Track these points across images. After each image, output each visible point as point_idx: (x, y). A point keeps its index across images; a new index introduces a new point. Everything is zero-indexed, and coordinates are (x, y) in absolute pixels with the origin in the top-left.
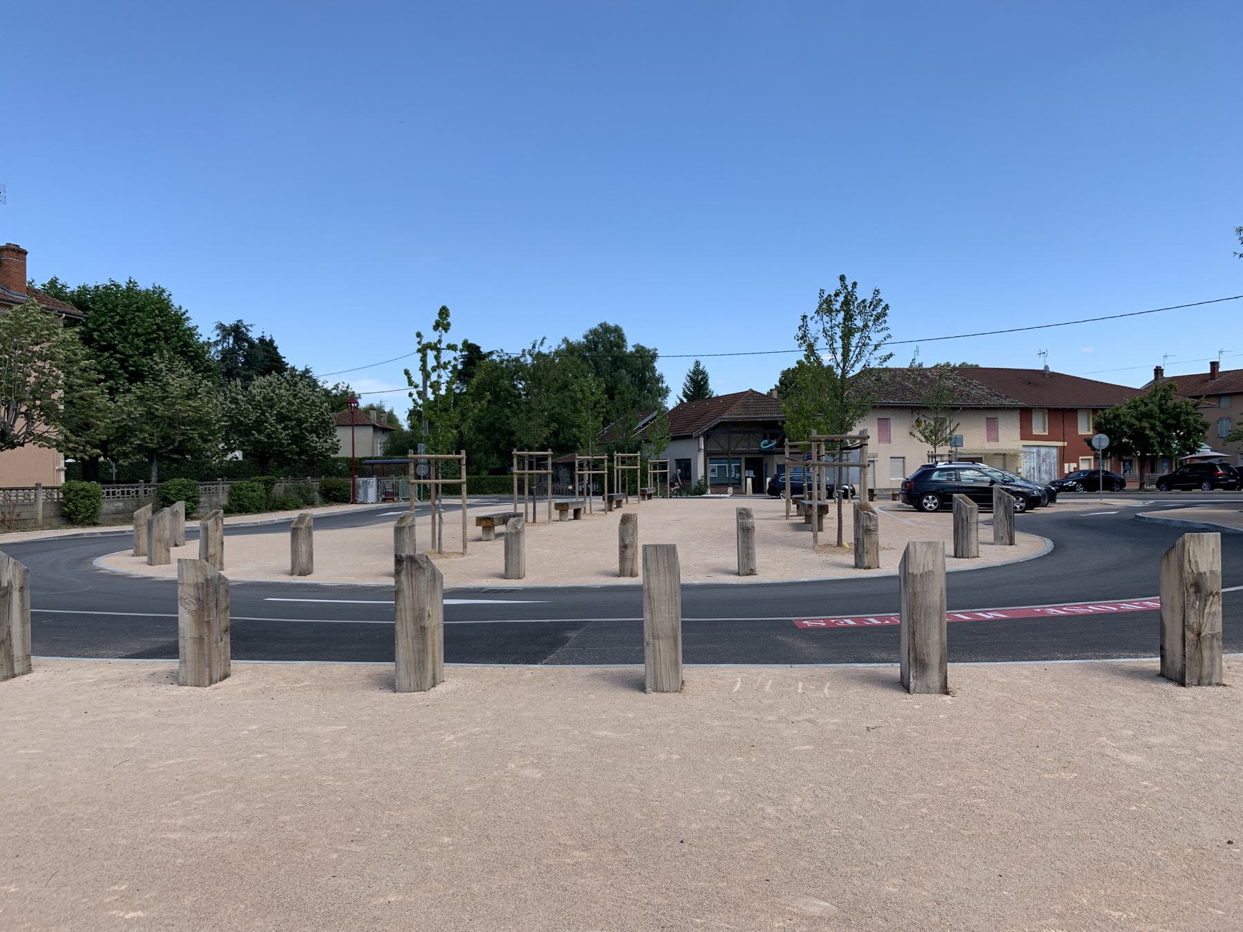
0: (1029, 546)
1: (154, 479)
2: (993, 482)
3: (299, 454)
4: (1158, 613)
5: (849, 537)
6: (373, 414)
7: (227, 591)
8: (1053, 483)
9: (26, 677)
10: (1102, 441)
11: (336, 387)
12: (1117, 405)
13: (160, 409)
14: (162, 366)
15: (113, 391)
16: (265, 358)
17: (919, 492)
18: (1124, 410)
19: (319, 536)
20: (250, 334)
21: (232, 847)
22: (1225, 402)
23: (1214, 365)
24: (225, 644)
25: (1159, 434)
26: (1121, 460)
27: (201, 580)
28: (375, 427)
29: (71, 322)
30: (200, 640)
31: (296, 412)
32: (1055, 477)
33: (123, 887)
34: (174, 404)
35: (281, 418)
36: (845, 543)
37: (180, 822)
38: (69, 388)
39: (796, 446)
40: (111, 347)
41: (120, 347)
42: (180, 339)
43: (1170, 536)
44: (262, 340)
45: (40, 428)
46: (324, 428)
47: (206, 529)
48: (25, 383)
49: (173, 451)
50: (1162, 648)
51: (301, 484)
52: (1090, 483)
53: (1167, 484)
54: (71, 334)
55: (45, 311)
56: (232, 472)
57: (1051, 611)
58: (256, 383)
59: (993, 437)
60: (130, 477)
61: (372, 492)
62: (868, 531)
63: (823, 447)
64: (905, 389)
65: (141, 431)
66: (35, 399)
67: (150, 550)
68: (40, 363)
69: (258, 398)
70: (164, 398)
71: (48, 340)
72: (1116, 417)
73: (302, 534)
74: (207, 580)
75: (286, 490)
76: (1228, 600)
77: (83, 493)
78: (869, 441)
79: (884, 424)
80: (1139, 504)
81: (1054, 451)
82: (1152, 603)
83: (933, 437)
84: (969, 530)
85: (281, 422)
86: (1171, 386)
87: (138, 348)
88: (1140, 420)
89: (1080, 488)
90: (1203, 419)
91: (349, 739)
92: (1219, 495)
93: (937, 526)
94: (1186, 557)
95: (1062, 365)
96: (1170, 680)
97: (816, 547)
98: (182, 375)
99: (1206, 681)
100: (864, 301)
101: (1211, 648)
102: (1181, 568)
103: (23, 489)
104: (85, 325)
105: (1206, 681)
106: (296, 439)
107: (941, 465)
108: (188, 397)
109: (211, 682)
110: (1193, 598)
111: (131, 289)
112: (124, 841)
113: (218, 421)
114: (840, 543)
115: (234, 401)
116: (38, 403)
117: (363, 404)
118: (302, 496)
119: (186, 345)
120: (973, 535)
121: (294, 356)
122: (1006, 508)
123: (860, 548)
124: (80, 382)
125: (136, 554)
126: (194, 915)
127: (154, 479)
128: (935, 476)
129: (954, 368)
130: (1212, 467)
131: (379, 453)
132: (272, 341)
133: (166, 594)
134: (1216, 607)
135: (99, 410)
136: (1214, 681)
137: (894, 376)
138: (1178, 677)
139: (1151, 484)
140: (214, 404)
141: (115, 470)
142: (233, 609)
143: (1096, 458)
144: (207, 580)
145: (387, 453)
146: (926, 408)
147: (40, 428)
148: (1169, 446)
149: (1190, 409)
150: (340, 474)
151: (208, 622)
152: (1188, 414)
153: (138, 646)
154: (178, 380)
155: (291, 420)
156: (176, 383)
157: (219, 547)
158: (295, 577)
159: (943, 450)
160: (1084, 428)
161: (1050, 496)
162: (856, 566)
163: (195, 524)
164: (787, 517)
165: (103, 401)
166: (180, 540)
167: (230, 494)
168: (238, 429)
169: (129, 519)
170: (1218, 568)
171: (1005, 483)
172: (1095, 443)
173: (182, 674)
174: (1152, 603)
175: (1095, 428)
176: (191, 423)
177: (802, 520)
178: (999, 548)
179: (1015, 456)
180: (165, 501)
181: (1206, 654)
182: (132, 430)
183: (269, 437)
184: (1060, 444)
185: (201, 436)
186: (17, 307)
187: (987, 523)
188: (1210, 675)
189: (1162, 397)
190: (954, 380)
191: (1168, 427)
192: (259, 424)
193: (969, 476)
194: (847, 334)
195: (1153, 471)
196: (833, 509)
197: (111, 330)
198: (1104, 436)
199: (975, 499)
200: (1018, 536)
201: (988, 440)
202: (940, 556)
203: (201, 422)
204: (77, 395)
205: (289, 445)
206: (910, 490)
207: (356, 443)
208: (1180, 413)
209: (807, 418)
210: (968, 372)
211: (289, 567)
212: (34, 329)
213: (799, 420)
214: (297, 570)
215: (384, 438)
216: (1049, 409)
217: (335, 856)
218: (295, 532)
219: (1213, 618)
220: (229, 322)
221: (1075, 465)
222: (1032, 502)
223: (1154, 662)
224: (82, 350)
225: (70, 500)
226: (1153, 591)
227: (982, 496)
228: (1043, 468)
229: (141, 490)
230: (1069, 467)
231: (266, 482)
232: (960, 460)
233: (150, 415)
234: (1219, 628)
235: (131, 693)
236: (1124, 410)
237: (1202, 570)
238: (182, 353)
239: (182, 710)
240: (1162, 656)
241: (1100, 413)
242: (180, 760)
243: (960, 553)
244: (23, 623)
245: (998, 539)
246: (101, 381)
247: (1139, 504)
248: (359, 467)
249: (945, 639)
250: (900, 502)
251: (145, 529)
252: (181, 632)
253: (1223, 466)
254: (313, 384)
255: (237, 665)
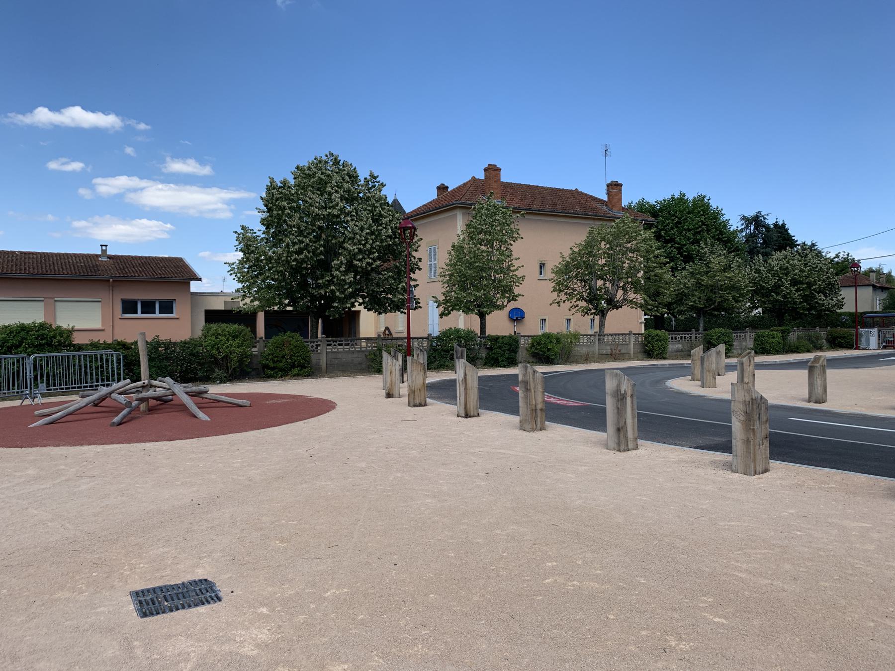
1: (701, 328)
3: (809, 310)
6: (873, 276)
7: (767, 409)
9: (635, 452)
11: (837, 256)
13: (705, 280)
14: (706, 250)
15: (674, 269)
16: (779, 238)
19: (832, 374)
20: (767, 221)
21: (785, 594)
23: (614, 188)
24: (765, 448)
27: (748, 399)
28: (874, 287)
29: (648, 226)
30: (747, 442)
31: (807, 277)
33: (710, 600)
34: (715, 276)
35: (794, 282)
37: (744, 566)
38: (648, 270)
40: (672, 240)
41: (677, 239)
42: (717, 230)
44: (776, 225)
45: (631, 296)
46: (831, 289)
47: (742, 364)
48: (622, 268)
49: (714, 309)
51: (812, 333)
54: (648, 234)
55: (634, 221)
56: (754, 324)
58: (775, 257)
60: (686, 327)
61: (874, 341)
65: (693, 296)
66: (628, 277)
67: (702, 377)
68: (631, 255)
69: (776, 268)
70: (707, 272)
71: (636, 239)
73: (817, 372)
74: (752, 399)
75: (799, 338)
77: (657, 338)
85: (794, 286)
87: (689, 239)
91: (876, 536)
98: (720, 255)
103: (612, 335)
104: (656, 227)
106: (806, 298)
108: (724, 271)
109: (755, 474)
111: (682, 199)
112: (707, 569)
113: (746, 287)
115: (758, 271)
116: (630, 280)
117: (864, 267)
118: (812, 342)
119: (721, 233)
121: (801, 234)
124: (655, 265)
125: (693, 379)
126: (762, 634)
127: (701, 328)
131: (878, 308)
132: (784, 225)
133: (722, 408)
135: (666, 283)
140: (743, 275)
141: (674, 323)
142: (772, 422)
144: (752, 399)
145: (886, 308)
147: (631, 296)
150: (843, 325)
151: (753, 430)
153: (701, 442)
154: (717, 258)
155: (803, 284)
156: (716, 261)
157: (751, 378)
158: (811, 404)
163: (733, 361)
165: (668, 276)
166: (722, 371)
167: (755, 340)
168: (760, 292)
169: (689, 356)
173: (735, 463)
176: (727, 289)
180: (709, 345)
182: (686, 295)
183: (785, 297)
185: (734, 298)
186: (618, 221)
192: (777, 288)
197: (672, 229)
203: (734, 288)
204: (653, 274)
205: (801, 303)
207: (856, 300)
211: (807, 396)
212: (628, 233)
214: (813, 399)
215: (884, 295)
217: (872, 624)
218: (811, 369)
220: (750, 214)
224: (655, 244)
225: (649, 342)
229: (693, 336)
231: (783, 332)
233: (699, 285)
235: (700, 471)
238: (718, 239)
239: (736, 489)
242: (739, 524)
244: (633, 418)
246: (667, 263)
248: (861, 320)
251: (698, 363)
252: (733, 435)
254: (819, 254)
255: (774, 464)
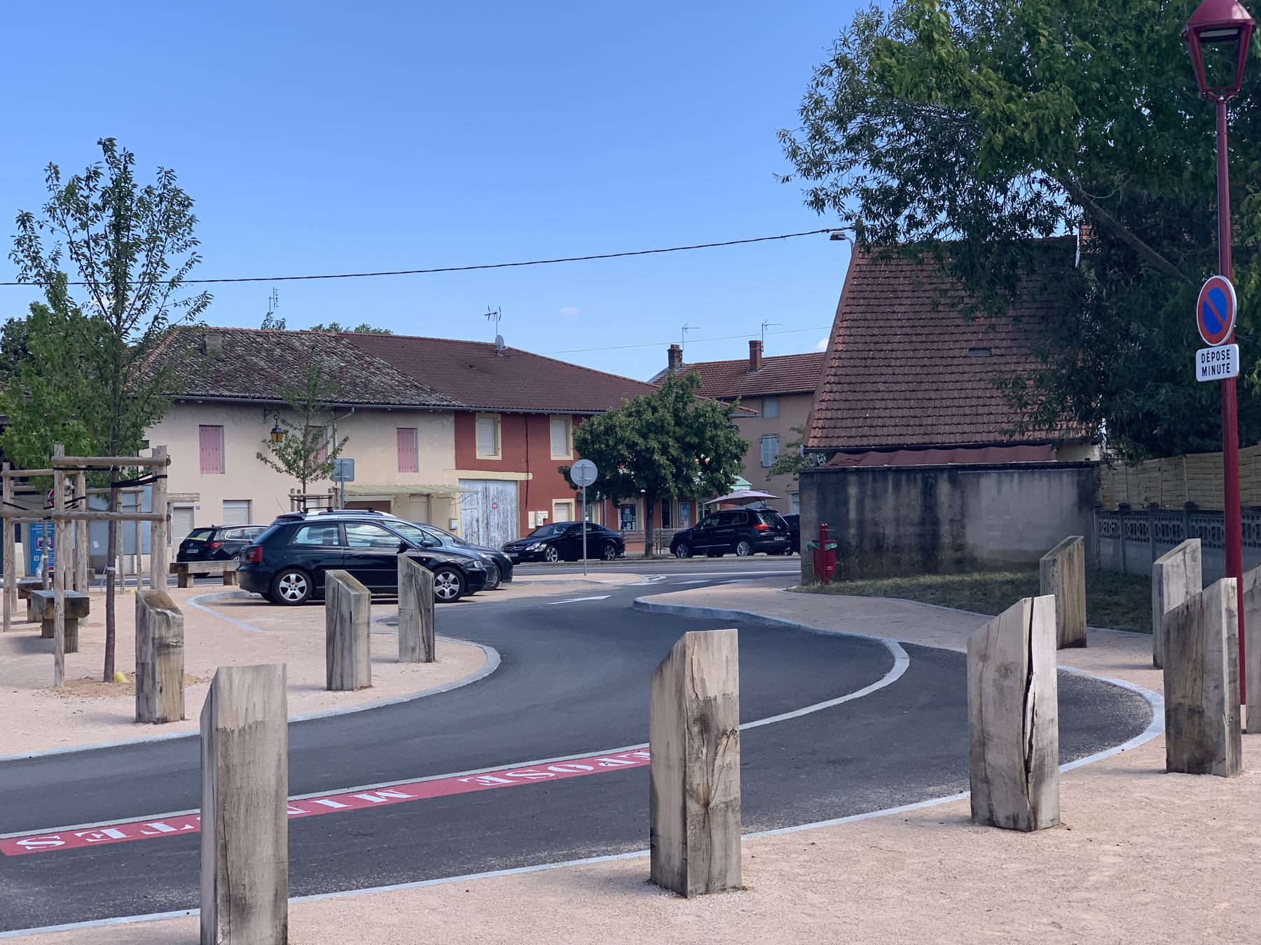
0: (461, 662)
2: (404, 547)
4: (644, 775)
5: (126, 663)
8: (508, 548)
10: (586, 472)
12: (611, 409)
17: (273, 567)
18: (621, 418)
22: (770, 408)
23: (755, 346)
25: (674, 461)
26: (617, 506)
32: (513, 536)
36: (119, 674)
39: (24, 480)
43: (653, 633)
50: (653, 833)
52: (569, 546)
53: (689, 545)
57: (488, 779)
59: (408, 462)
62: (163, 648)
63: (82, 480)
64: (252, 369)
72: (610, 430)
76: (751, 746)
78: (168, 470)
79: (210, 433)
80: (643, 580)
81: (512, 490)
82: (642, 754)
83: (300, 462)
84: (354, 637)
86: (691, 380)
88: (645, 437)
89: (553, 555)
90: (739, 436)
92: (763, 563)
93: (296, 630)
94: (688, 673)
95: (525, 336)
96: (665, 888)
97: (62, 684)
99: (718, 885)
100: (149, 191)
101: (725, 826)
102: (680, 691)
105: (718, 885)
107: (313, 515)
110: (697, 742)
114: (109, 675)
120: (361, 648)
122: (420, 595)
123: (148, 682)
128: (302, 537)
129: (346, 335)
130: (751, 517)
134: (731, 755)
136: (730, 883)
137: (232, 345)
138: (676, 882)
139: (663, 546)
143: (579, 502)
146: (287, 408)
148: (689, 481)
149: (720, 418)
152: (716, 426)
159: (320, 486)
160: (560, 448)
161: (502, 569)
162: (140, 719)
164: (6, 624)
170: (734, 689)
171: (425, 547)
172: (575, 477)
174: (642, 754)
175: (577, 448)
177: (36, 630)
178: (408, 668)
179: (447, 498)
181: (717, 836)
184: (522, 476)
187: (391, 622)
188: (724, 873)
189: (679, 398)
190: (342, 356)
191: (687, 448)
193: (363, 536)
194: (122, 256)
195: (666, 523)
196: (97, 607)
198: (589, 464)
199: (365, 578)
200: (442, 645)
201: (401, 469)
202: (277, 693)
206: (255, 563)
208: (704, 425)
209: (49, 421)
210: (369, 343)
213: (32, 426)
216: (504, 414)
219: (725, 775)
221: (545, 514)
222: (471, 581)
223: (638, 860)
226: (640, 734)
227: (378, 573)
228: (494, 520)
230: (536, 518)
232: (350, 505)
234: (735, 792)
236: (621, 418)
237: (711, 694)
240: (653, 848)
241: (584, 421)
243: (337, 682)
245: (405, 653)
247: (643, 580)
249: (284, 852)
250: (235, 588)
253: (767, 513)
